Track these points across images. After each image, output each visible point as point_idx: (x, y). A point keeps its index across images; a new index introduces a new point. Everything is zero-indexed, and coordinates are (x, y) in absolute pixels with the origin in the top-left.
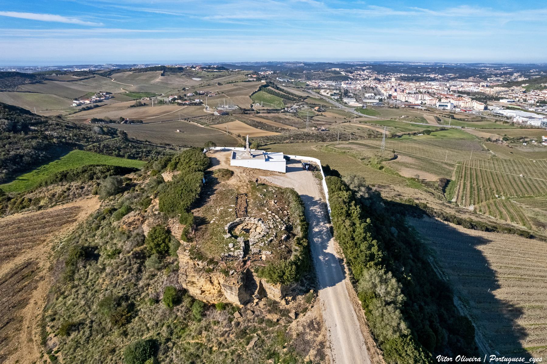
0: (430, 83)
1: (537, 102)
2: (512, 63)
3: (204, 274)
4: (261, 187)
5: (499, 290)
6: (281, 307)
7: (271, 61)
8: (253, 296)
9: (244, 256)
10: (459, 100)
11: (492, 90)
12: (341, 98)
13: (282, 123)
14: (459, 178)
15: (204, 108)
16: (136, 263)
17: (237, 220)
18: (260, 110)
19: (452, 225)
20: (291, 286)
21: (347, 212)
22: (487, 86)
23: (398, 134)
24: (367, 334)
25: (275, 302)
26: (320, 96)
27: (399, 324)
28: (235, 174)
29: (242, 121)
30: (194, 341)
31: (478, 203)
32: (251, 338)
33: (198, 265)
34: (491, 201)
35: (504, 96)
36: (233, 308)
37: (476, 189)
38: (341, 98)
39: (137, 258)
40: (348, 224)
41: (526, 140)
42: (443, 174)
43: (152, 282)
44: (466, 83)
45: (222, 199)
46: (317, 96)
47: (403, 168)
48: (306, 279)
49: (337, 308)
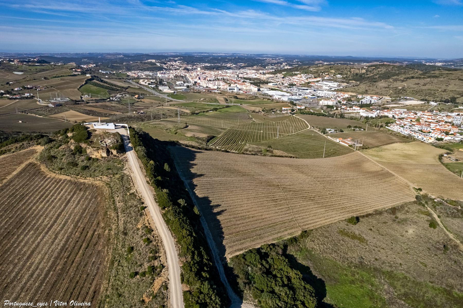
0: (226, 71)
2: (285, 54)
7: (92, 52)
11: (265, 76)
12: (157, 86)
13: (109, 110)
18: (89, 100)
19: (189, 148)
23: (196, 112)
26: (139, 85)
35: (271, 81)
38: (157, 86)
41: (274, 110)
46: (137, 86)
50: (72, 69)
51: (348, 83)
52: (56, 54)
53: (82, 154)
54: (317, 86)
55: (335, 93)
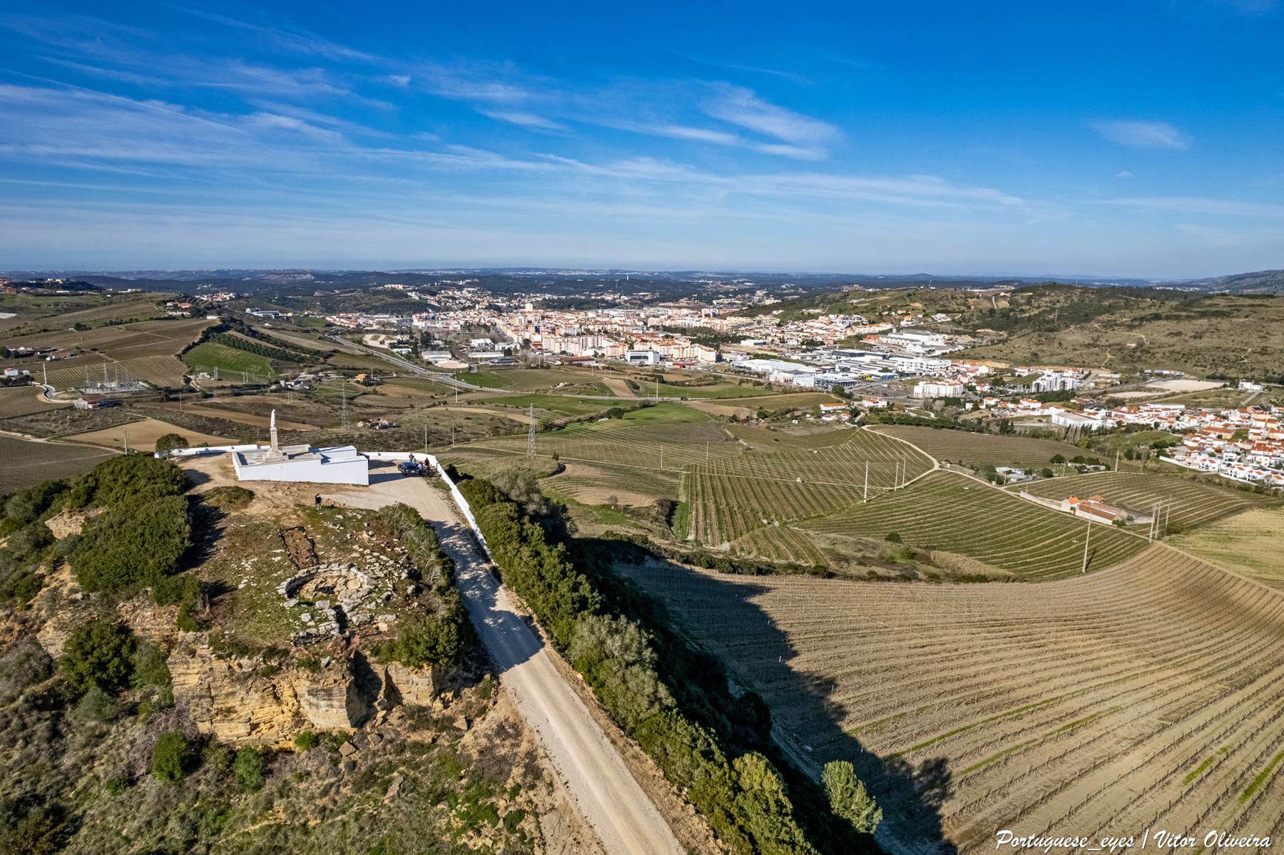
0: (606, 311)
1: (802, 344)
3: (258, 683)
4: (328, 512)
5: (796, 660)
6: (435, 716)
7: (226, 268)
8: (376, 704)
9: (342, 631)
10: (668, 345)
11: (725, 322)
14: (693, 496)
15: (38, 391)
16: (39, 719)
17: (301, 573)
18: (211, 389)
19: (698, 569)
20: (447, 672)
21: (520, 533)
22: (715, 315)
23: (557, 422)
24: (604, 720)
25: (422, 709)
27: (656, 691)
28: (258, 494)
29: (164, 420)
30: (257, 827)
31: (736, 538)
32: (390, 781)
33: (240, 666)
34: (757, 531)
35: (747, 334)
36: (335, 739)
37: (727, 513)
38: (415, 351)
39: (40, 708)
40: (528, 554)
41: (797, 413)
42: (662, 493)
43: (97, 750)
44: (676, 311)
45: (246, 544)
46: (358, 350)
47: (581, 488)
48: (471, 659)
49: (541, 696)
50: (165, 302)
51: (974, 335)
52: (126, 273)
53: (134, 696)
54: (886, 344)
55: (949, 362)
